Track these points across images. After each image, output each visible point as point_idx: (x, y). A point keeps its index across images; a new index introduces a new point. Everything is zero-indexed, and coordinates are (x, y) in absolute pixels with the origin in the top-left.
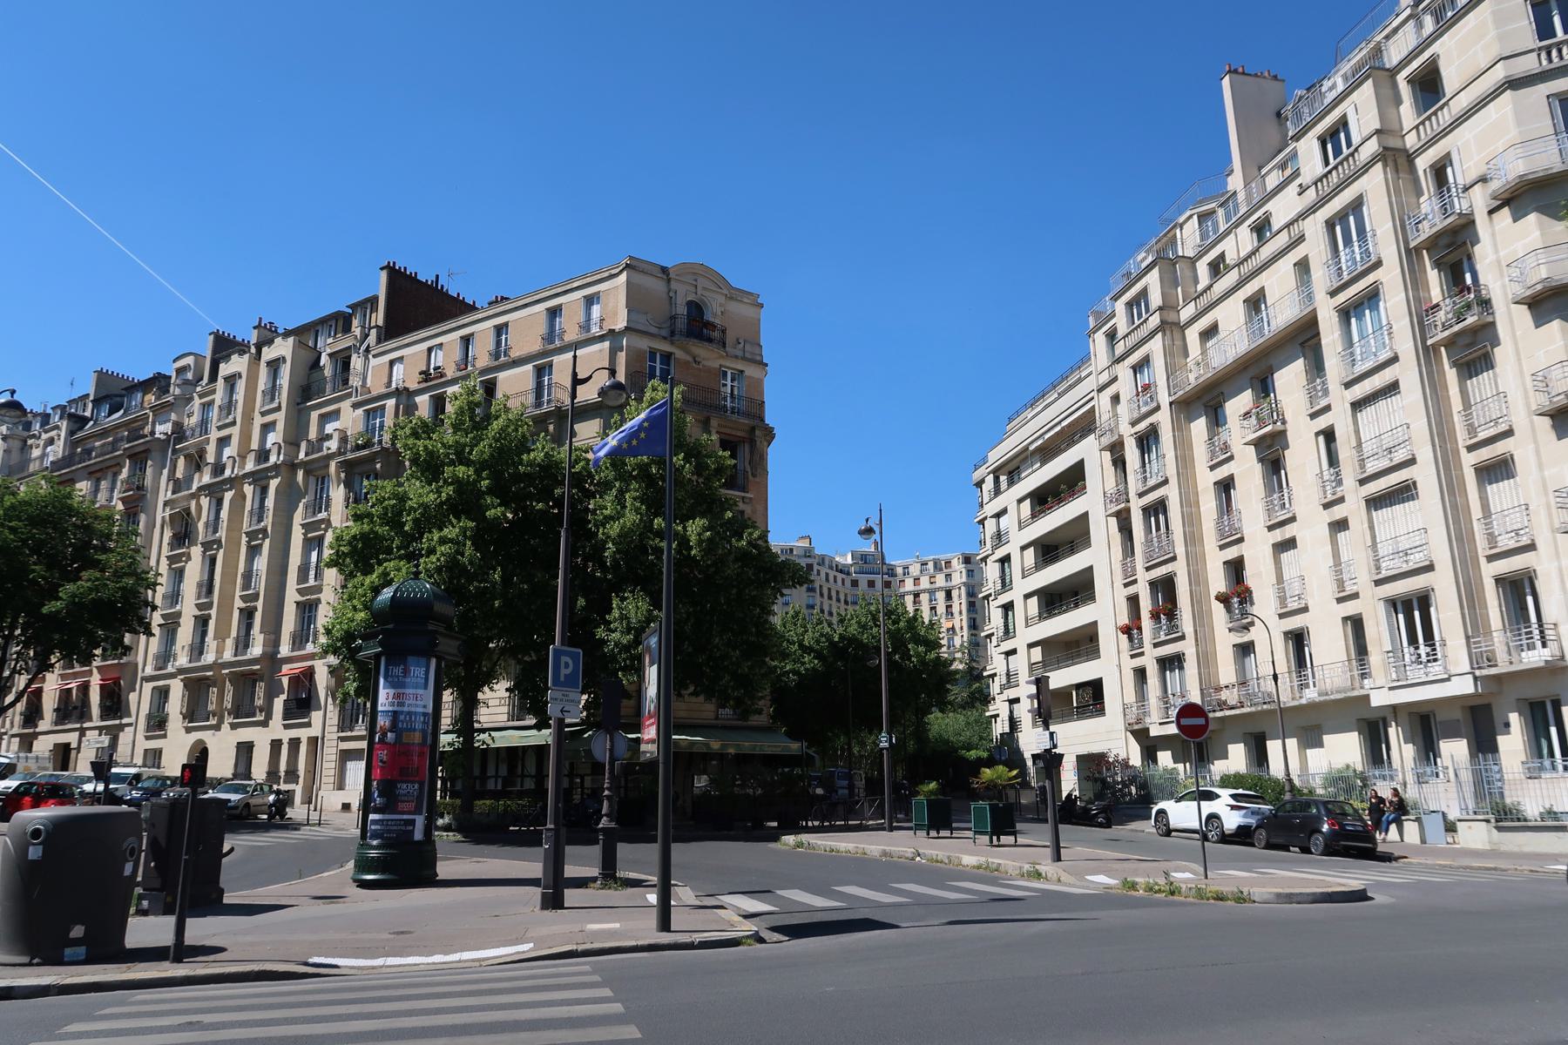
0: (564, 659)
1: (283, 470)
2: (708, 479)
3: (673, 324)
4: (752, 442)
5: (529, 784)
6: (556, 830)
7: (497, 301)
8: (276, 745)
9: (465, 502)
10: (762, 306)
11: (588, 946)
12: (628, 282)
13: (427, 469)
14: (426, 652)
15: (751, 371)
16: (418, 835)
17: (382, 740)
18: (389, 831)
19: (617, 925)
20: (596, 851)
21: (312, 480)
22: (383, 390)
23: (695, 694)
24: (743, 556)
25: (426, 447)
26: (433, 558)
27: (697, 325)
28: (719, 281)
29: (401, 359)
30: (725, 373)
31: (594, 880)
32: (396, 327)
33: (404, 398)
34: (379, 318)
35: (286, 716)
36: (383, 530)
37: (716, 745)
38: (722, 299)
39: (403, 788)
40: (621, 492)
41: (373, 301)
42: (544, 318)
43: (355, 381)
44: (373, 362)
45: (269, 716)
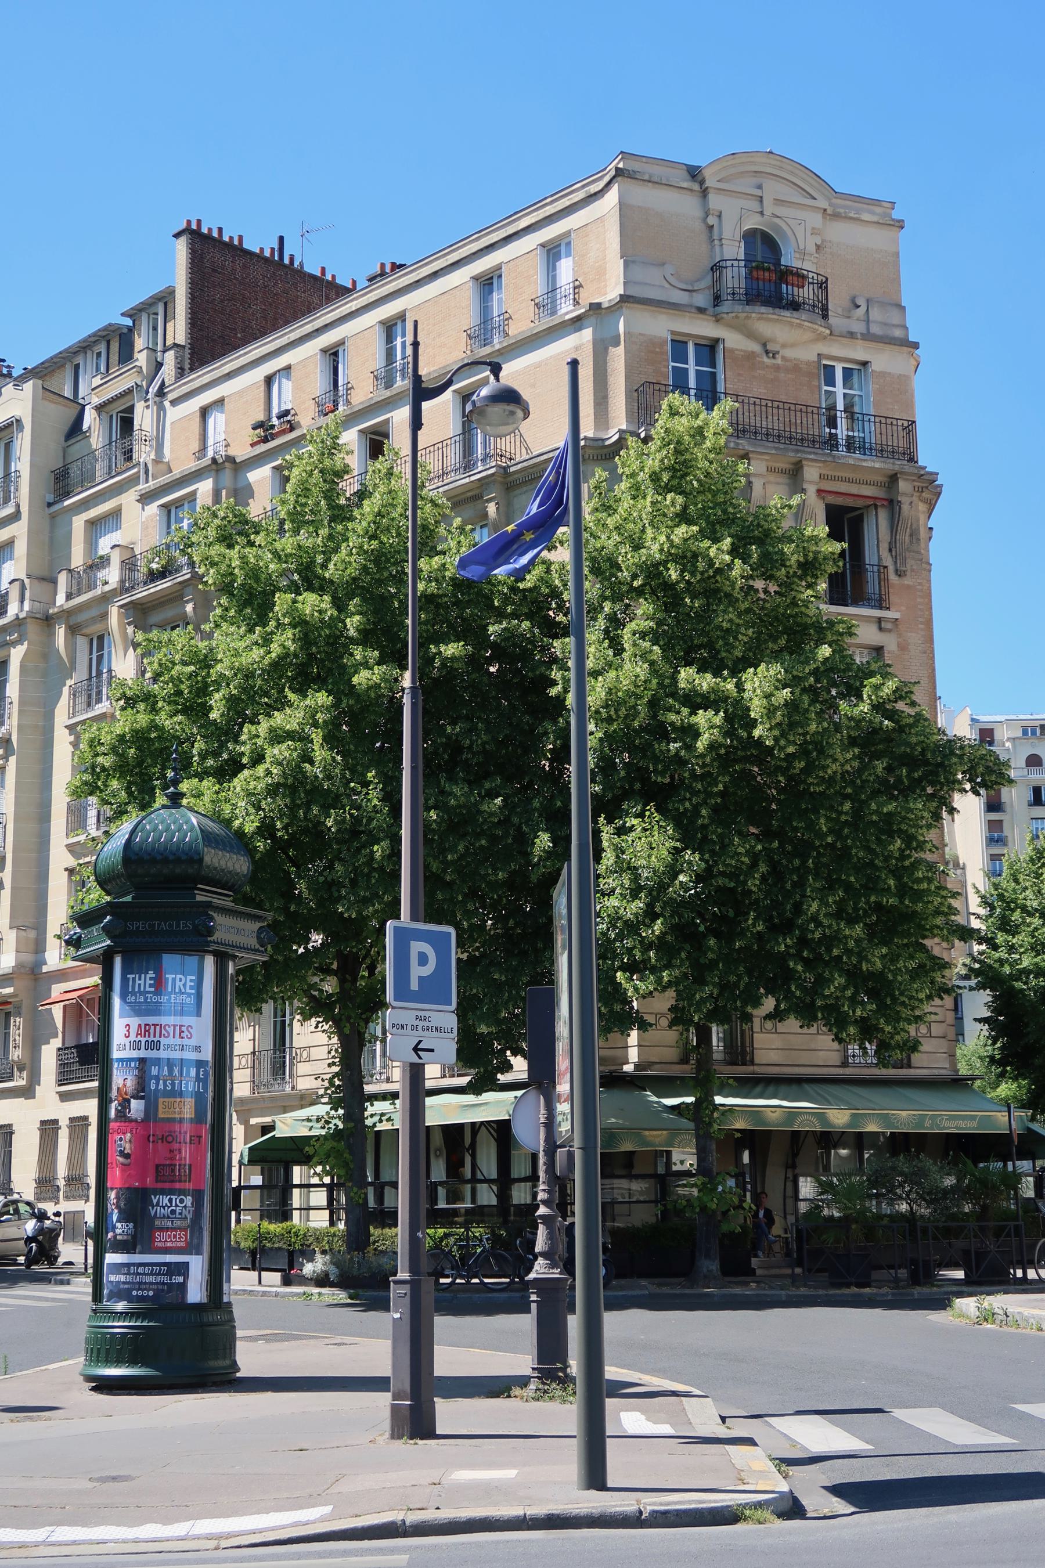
0: (417, 947)
1: (32, 629)
2: (787, 586)
3: (717, 281)
4: (892, 504)
5: (487, 1196)
6: (414, 1285)
7: (383, 274)
8: (49, 1128)
9: (316, 662)
10: (900, 225)
11: (429, 1515)
12: (622, 204)
13: (247, 603)
14: (195, 941)
15: (883, 361)
16: (196, 1293)
17: (122, 1114)
18: (140, 1285)
19: (511, 1473)
20: (524, 1325)
21: (82, 643)
22: (192, 465)
23: (777, 1015)
24: (867, 740)
25: (243, 558)
26: (260, 770)
27: (769, 279)
28: (809, 183)
29: (220, 402)
30: (829, 371)
31: (523, 1382)
32: (207, 345)
33: (227, 476)
34: (178, 330)
35: (63, 1079)
36: (170, 722)
37: (839, 1118)
38: (815, 220)
39: (162, 1204)
40: (615, 622)
41: (166, 298)
42: (469, 296)
43: (143, 454)
44: (173, 414)
45: (34, 1078)
